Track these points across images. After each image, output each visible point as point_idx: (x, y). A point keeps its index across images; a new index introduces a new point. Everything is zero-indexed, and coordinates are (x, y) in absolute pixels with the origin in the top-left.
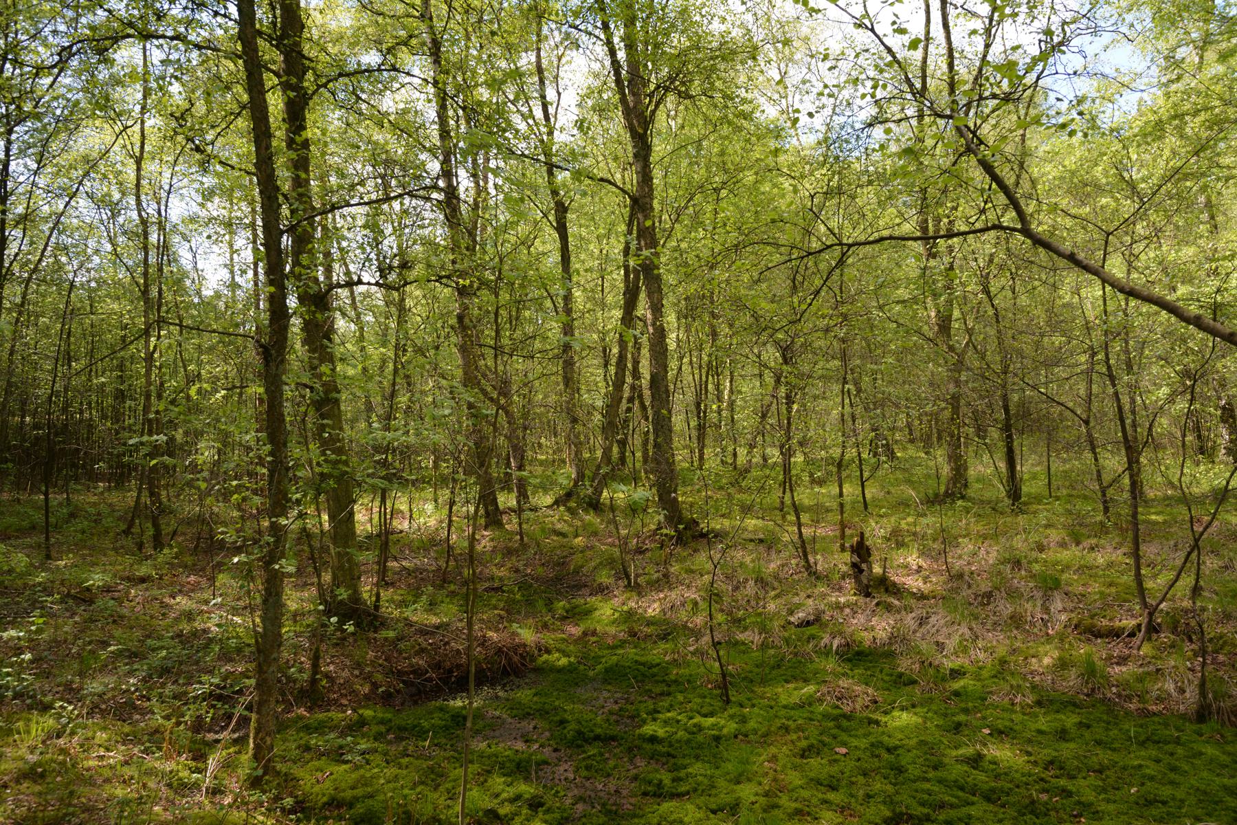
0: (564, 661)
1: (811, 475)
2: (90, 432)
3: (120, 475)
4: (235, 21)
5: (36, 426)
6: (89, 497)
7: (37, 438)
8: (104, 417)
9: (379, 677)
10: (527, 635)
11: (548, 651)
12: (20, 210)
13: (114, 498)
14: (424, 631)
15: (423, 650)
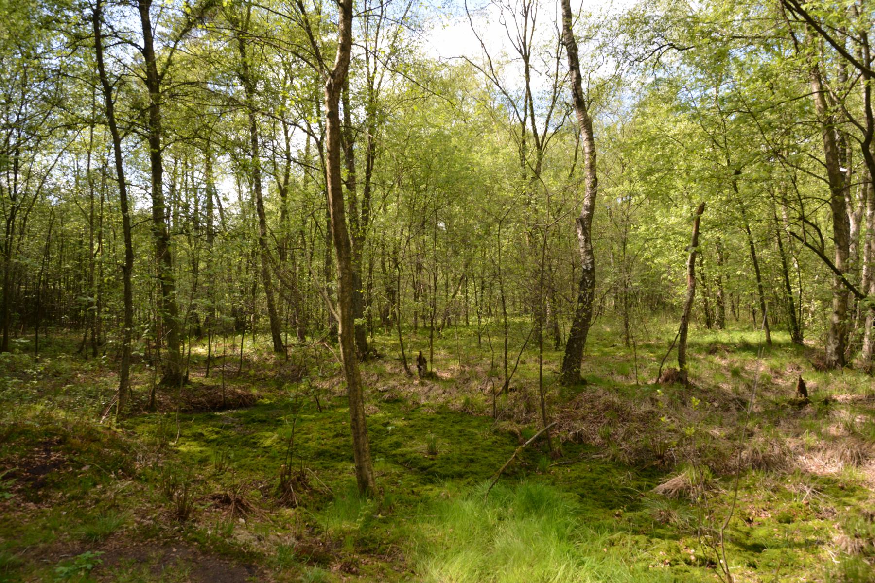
0: (269, 402)
1: (663, 462)
2: (60, 298)
3: (77, 323)
4: (140, 48)
5: (26, 293)
6: (15, 244)
7: (27, 300)
8: (68, 288)
9: (183, 404)
10: (254, 391)
11: (263, 398)
12: (748, 482)
13: (74, 336)
14: (208, 388)
15: (204, 395)
